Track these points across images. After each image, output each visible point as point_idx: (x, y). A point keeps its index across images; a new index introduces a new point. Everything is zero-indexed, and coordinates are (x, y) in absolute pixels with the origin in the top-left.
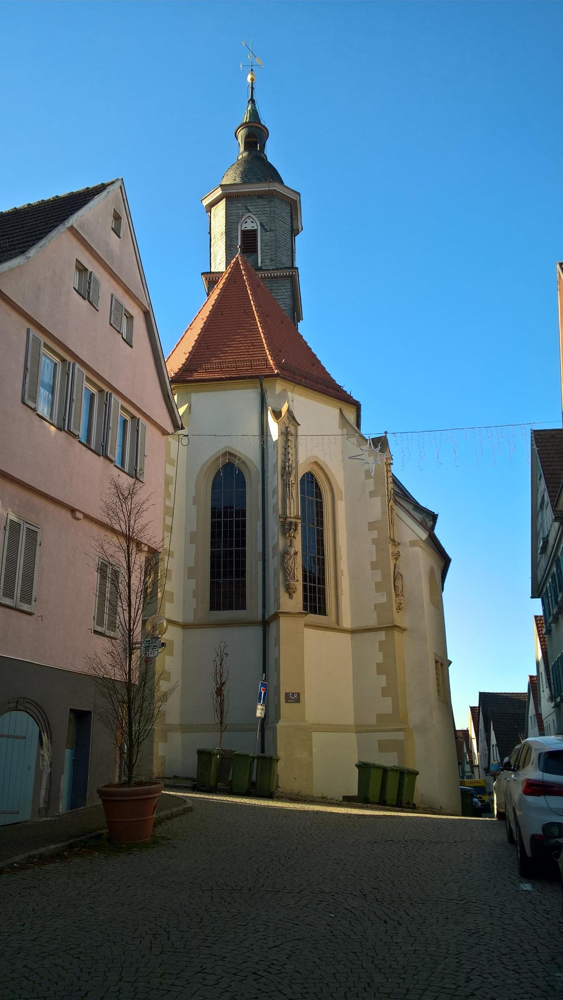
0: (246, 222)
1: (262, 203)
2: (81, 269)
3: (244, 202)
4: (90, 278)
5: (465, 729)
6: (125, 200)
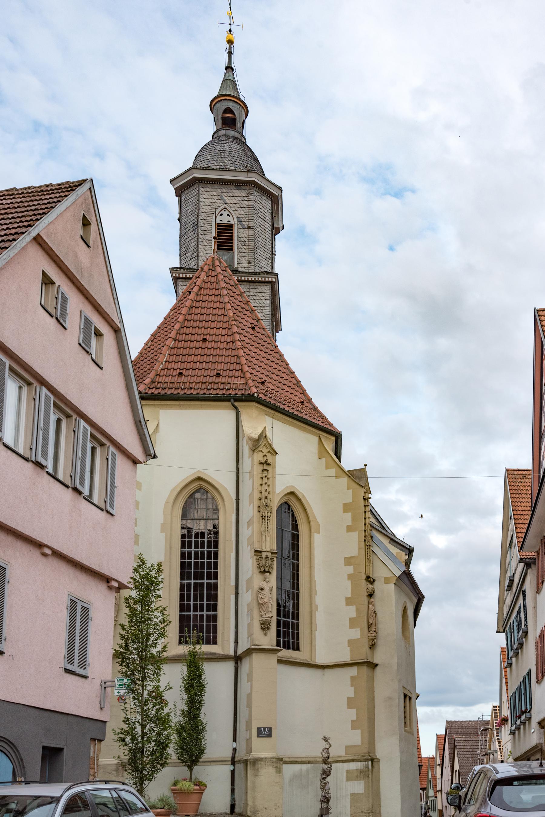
0: (221, 215)
3: (219, 190)
6: (95, 204)
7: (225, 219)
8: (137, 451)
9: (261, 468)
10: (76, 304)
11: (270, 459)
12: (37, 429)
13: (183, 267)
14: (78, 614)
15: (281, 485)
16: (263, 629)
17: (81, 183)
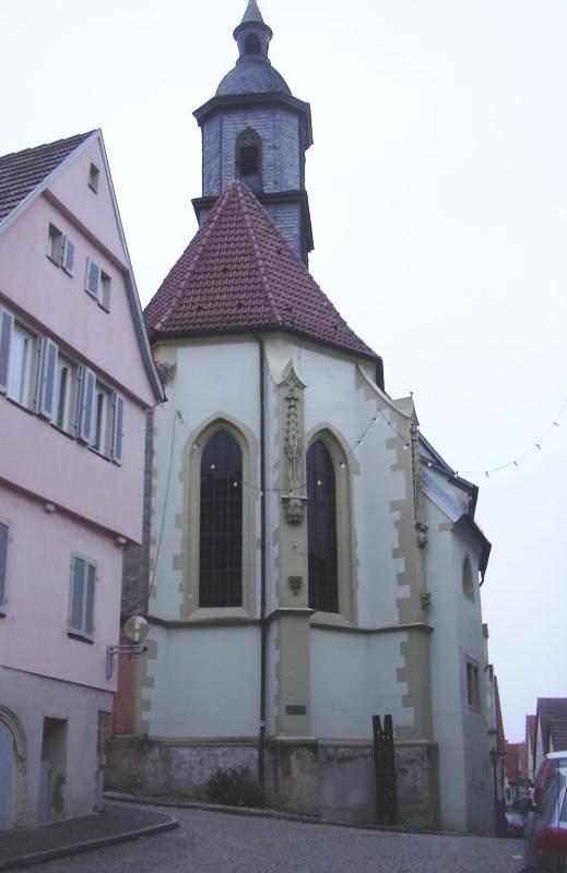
9: (287, 404)
10: (82, 253)
11: (297, 393)
12: (40, 380)
14: (84, 575)
15: (312, 422)
16: (292, 588)
17: (89, 134)
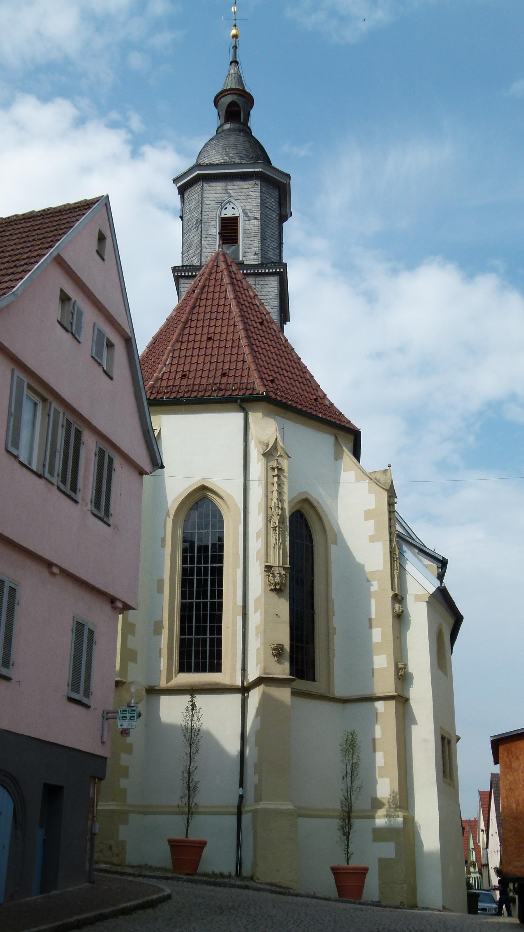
0: (226, 208)
1: (246, 187)
2: (65, 298)
4: (74, 308)
5: (472, 819)
7: (229, 213)
8: (144, 462)
10: (90, 316)
13: (185, 264)
